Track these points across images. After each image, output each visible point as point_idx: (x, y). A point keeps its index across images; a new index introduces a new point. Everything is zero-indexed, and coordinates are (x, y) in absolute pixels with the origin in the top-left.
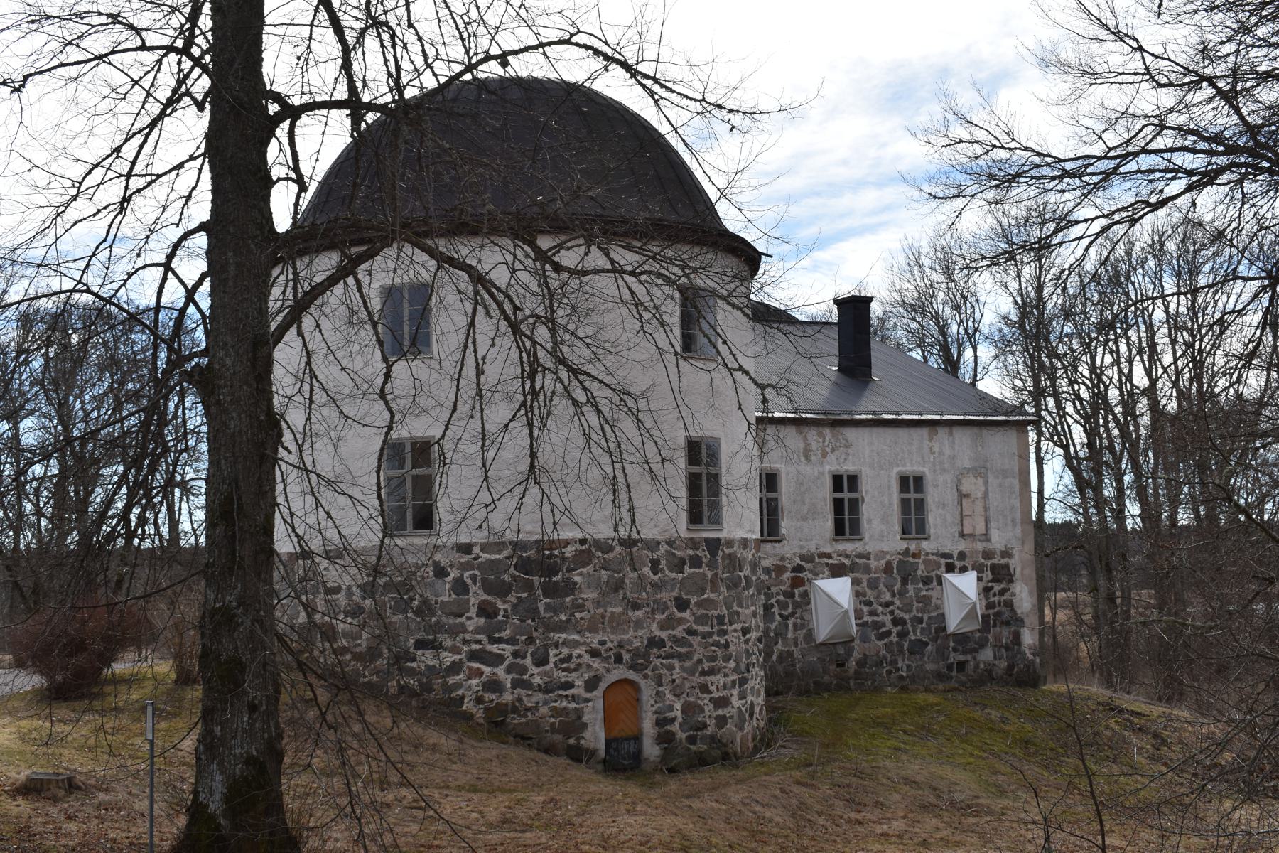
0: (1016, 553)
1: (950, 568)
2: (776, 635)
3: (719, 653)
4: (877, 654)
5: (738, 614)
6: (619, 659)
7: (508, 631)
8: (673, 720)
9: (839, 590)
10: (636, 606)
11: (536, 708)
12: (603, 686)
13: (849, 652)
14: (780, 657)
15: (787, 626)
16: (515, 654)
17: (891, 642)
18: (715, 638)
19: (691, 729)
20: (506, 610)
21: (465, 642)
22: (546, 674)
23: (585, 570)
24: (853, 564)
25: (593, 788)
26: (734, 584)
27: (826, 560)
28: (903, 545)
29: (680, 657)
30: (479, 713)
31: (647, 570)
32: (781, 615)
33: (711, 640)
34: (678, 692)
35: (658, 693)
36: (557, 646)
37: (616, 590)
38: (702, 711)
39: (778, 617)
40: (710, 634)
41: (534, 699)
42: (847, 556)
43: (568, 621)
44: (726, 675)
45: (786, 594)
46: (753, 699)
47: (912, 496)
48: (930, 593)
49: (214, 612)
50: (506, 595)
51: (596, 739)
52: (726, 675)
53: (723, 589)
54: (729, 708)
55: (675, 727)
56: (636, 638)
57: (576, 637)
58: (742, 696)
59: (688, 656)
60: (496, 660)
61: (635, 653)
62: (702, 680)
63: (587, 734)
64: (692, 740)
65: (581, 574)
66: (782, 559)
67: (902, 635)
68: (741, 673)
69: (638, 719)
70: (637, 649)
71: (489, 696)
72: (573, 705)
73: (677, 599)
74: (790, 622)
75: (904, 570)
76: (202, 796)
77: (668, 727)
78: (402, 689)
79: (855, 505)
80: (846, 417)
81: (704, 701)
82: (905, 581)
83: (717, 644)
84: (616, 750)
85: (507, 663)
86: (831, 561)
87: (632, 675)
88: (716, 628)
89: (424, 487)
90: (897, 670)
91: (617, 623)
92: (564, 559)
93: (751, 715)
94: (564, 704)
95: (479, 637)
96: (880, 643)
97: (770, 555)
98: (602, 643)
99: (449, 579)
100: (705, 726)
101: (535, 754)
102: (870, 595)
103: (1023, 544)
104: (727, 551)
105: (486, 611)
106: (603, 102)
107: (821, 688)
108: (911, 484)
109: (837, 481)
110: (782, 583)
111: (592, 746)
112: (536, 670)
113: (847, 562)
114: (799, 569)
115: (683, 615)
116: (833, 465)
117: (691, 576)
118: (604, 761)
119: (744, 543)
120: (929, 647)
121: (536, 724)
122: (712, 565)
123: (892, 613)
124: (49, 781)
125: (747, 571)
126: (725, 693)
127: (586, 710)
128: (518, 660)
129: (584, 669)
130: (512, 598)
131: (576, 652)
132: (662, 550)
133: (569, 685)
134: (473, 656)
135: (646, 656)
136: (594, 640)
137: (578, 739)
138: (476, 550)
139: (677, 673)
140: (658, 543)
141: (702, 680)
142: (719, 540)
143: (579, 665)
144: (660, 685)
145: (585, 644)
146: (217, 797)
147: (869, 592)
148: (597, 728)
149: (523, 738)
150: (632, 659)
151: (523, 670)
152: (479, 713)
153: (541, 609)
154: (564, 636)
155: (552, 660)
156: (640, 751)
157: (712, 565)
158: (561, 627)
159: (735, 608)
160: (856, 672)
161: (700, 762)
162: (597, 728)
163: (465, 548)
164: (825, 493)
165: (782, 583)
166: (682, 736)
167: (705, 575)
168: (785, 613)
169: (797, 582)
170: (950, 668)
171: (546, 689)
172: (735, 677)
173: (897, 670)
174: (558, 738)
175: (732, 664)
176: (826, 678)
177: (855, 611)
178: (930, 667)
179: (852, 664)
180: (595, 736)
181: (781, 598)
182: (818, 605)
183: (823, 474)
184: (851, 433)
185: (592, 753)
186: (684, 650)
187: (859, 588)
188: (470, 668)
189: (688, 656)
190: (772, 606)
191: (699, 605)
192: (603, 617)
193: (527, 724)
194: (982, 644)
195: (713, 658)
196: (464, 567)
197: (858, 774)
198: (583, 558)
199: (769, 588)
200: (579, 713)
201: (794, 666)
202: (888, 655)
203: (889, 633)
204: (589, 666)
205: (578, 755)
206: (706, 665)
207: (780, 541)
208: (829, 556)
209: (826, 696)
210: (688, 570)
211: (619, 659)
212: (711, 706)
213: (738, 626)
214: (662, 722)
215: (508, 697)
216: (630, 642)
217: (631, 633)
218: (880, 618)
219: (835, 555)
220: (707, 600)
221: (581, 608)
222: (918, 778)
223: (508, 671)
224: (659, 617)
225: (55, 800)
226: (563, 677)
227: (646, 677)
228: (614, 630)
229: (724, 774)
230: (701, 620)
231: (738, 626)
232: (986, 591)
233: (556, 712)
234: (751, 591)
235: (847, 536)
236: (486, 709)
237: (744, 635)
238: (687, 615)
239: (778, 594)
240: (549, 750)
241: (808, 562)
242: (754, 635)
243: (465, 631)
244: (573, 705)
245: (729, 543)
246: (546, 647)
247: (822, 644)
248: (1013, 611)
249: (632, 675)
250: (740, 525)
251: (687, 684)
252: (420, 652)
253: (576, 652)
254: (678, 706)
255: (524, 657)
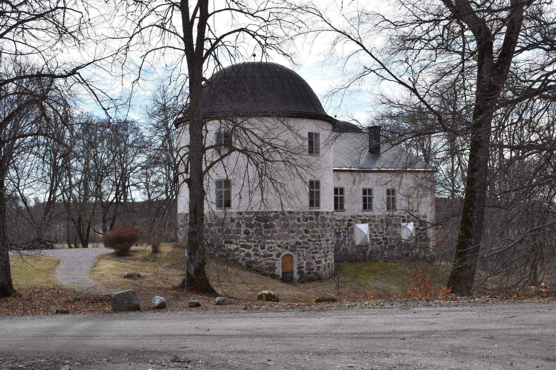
0: (428, 216)
1: (404, 221)
2: (342, 242)
3: (318, 247)
4: (377, 250)
5: (325, 235)
6: (287, 248)
7: (253, 239)
8: (303, 267)
9: (364, 228)
10: (292, 232)
11: (261, 262)
12: (282, 256)
13: (367, 249)
14: (343, 250)
15: (346, 239)
16: (255, 246)
17: (382, 246)
18: (317, 242)
19: (309, 270)
20: (252, 232)
21: (240, 242)
22: (264, 252)
23: (277, 221)
24: (369, 219)
25: (277, 284)
26: (324, 226)
27: (360, 218)
28: (387, 213)
29: (306, 248)
30: (244, 264)
31: (296, 221)
32: (344, 236)
33: (315, 243)
34: (305, 258)
35: (298, 259)
36: (268, 243)
37: (286, 227)
38: (312, 265)
39: (343, 237)
40: (316, 241)
41: (261, 259)
42: (367, 216)
43: (271, 236)
44: (320, 254)
45: (346, 229)
46: (330, 262)
47: (391, 196)
48: (397, 229)
49: (191, 232)
50: (253, 228)
51: (279, 272)
52: (320, 254)
53: (320, 227)
54: (321, 264)
55: (304, 269)
56: (292, 242)
57: (274, 241)
58: (326, 261)
59: (308, 248)
60: (249, 247)
61: (292, 246)
62: (312, 255)
63: (277, 270)
64: (309, 273)
65: (275, 222)
66: (345, 217)
67: (386, 243)
68: (325, 253)
69: (293, 266)
70: (292, 245)
71: (247, 258)
72: (272, 262)
73: (305, 230)
74: (347, 238)
75: (388, 221)
76: (189, 271)
77: (302, 269)
78: (220, 256)
79: (370, 199)
80: (369, 169)
81: (313, 261)
82: (387, 225)
83: (317, 244)
84: (285, 276)
85: (252, 248)
86: (361, 218)
87: (291, 253)
88: (317, 239)
89: (228, 194)
90: (384, 255)
91: (286, 237)
92: (270, 217)
93: (328, 267)
94: (270, 261)
95: (244, 240)
96: (378, 246)
97: (339, 215)
98: (282, 243)
99: (236, 222)
100: (313, 269)
101: (260, 276)
102: (375, 230)
103: (431, 213)
104: (322, 215)
105: (246, 232)
106: (286, 71)
107: (356, 260)
108: (391, 192)
109: (365, 192)
110: (344, 225)
111: (278, 274)
112: (261, 251)
113: (367, 218)
114: (350, 220)
115: (307, 235)
116: (363, 185)
117: (309, 223)
118: (282, 279)
119: (328, 213)
120: (396, 248)
121: (261, 267)
122: (317, 220)
123: (382, 236)
124: (134, 275)
125: (328, 222)
126: (320, 259)
127: (276, 263)
128: (256, 248)
129: (276, 251)
130: (254, 229)
131: (273, 246)
132: (301, 215)
133: (271, 256)
134: (242, 246)
135: (295, 247)
136: (279, 242)
137: (274, 272)
138: (244, 214)
139: (305, 253)
140: (300, 213)
141: (312, 255)
142: (319, 212)
143: (274, 249)
144: (299, 256)
145: (276, 243)
146: (192, 271)
147: (375, 229)
148: (280, 269)
149: (257, 271)
150: (291, 248)
151: (258, 251)
152: (244, 264)
153: (263, 232)
154: (270, 240)
155: (266, 248)
156: (293, 276)
157: (317, 220)
158: (269, 238)
159: (324, 233)
160: (369, 255)
161: (311, 280)
162: (280, 269)
163: (240, 213)
164: (360, 195)
165: (344, 225)
166: (306, 272)
167: (314, 223)
168: (345, 235)
169: (349, 225)
170: (402, 255)
171: (264, 257)
172: (323, 255)
173: (384, 255)
174: (268, 271)
175: (322, 251)
176: (359, 257)
177: (370, 235)
178: (396, 254)
179: (368, 253)
180: (279, 271)
181: (344, 230)
182: (356, 232)
183: (360, 189)
184: (370, 175)
185: (278, 276)
186: (307, 246)
187: (371, 227)
188: (241, 250)
189: (308, 248)
190: (341, 232)
191: (312, 232)
192: (282, 235)
193: (258, 267)
194: (415, 247)
195: (316, 249)
196: (240, 219)
197: (361, 285)
198: (276, 217)
199: (340, 227)
200: (274, 264)
201: (348, 253)
202: (381, 250)
203: (381, 243)
204: (277, 250)
205: (274, 276)
206: (314, 251)
207: (344, 211)
208: (361, 216)
209: (358, 263)
210: (309, 221)
211: (287, 248)
212: (315, 263)
213: (325, 239)
214: (300, 268)
215: (253, 259)
216: (290, 243)
217: (291, 240)
218: (379, 238)
219: (363, 216)
220: (315, 231)
221: (275, 232)
222: (380, 287)
223: (253, 251)
224: (300, 235)
225: (136, 279)
226: (270, 253)
227: (295, 254)
228: (285, 239)
229: (318, 284)
230: (313, 237)
231: (325, 239)
232: (417, 229)
233: (267, 264)
234: (329, 228)
235: (368, 210)
236: (246, 262)
237: (327, 241)
238: (308, 235)
239: (343, 229)
240: (265, 275)
241: (353, 218)
242: (330, 242)
243: (240, 238)
244: (272, 262)
245: (322, 213)
246: (264, 244)
247: (358, 246)
248: (427, 236)
249: (291, 253)
250: (326, 207)
251: (308, 256)
252: (226, 245)
253: (273, 246)
254: (305, 263)
255: (258, 247)
